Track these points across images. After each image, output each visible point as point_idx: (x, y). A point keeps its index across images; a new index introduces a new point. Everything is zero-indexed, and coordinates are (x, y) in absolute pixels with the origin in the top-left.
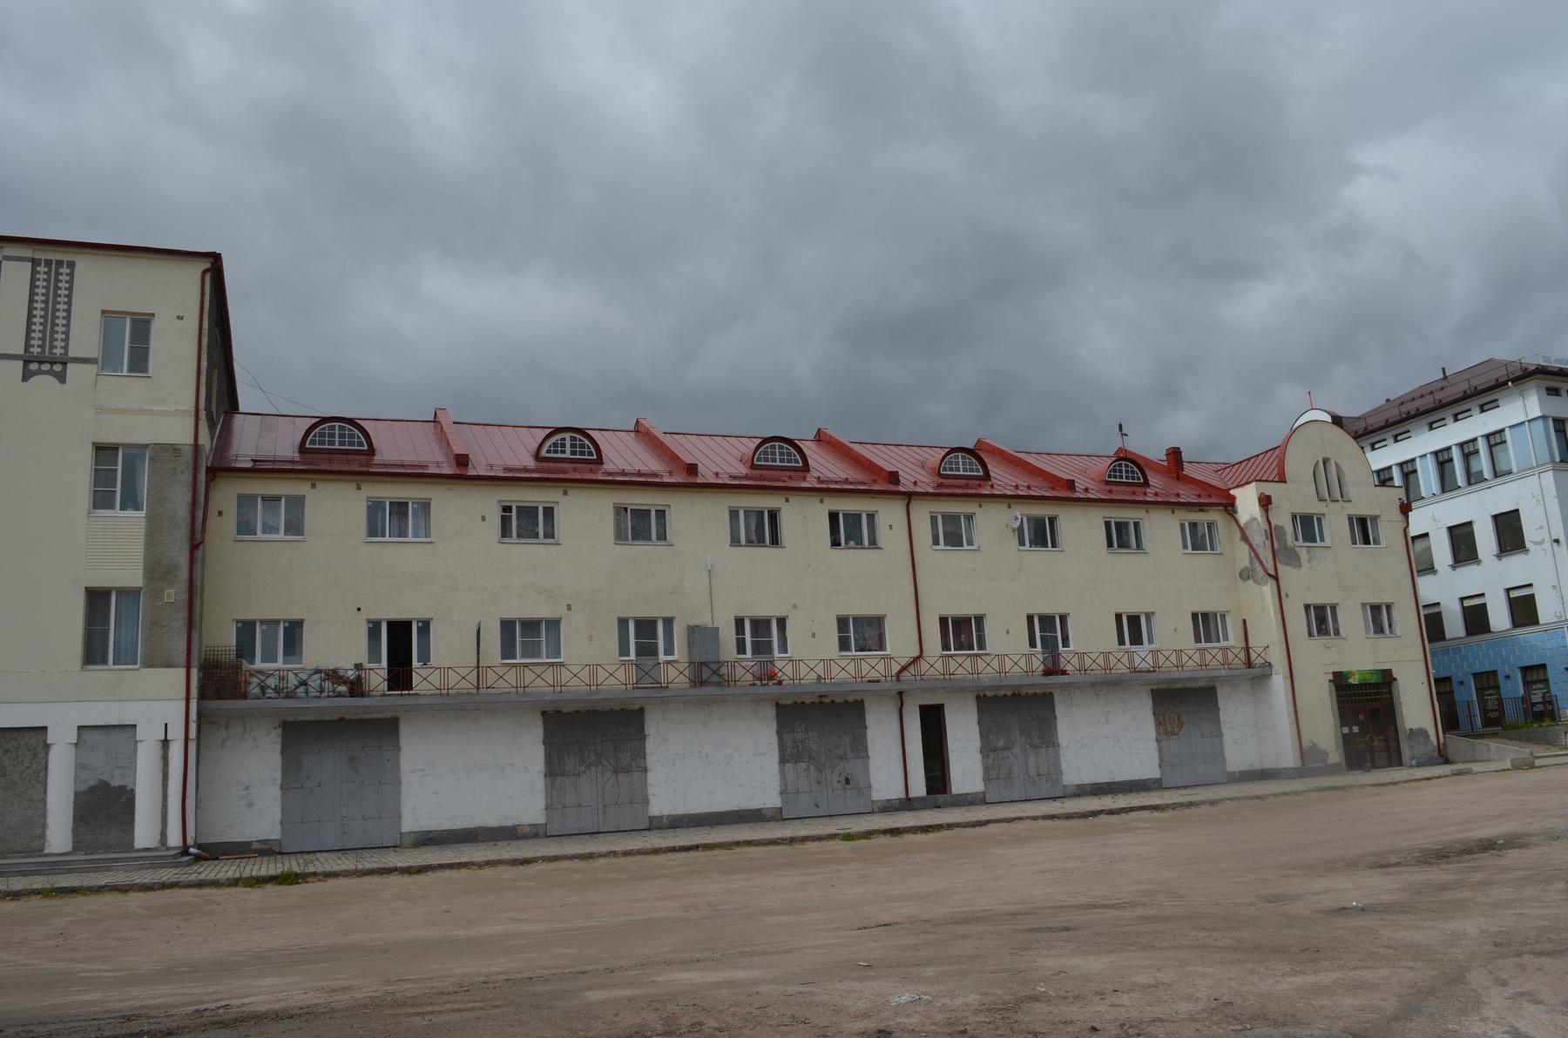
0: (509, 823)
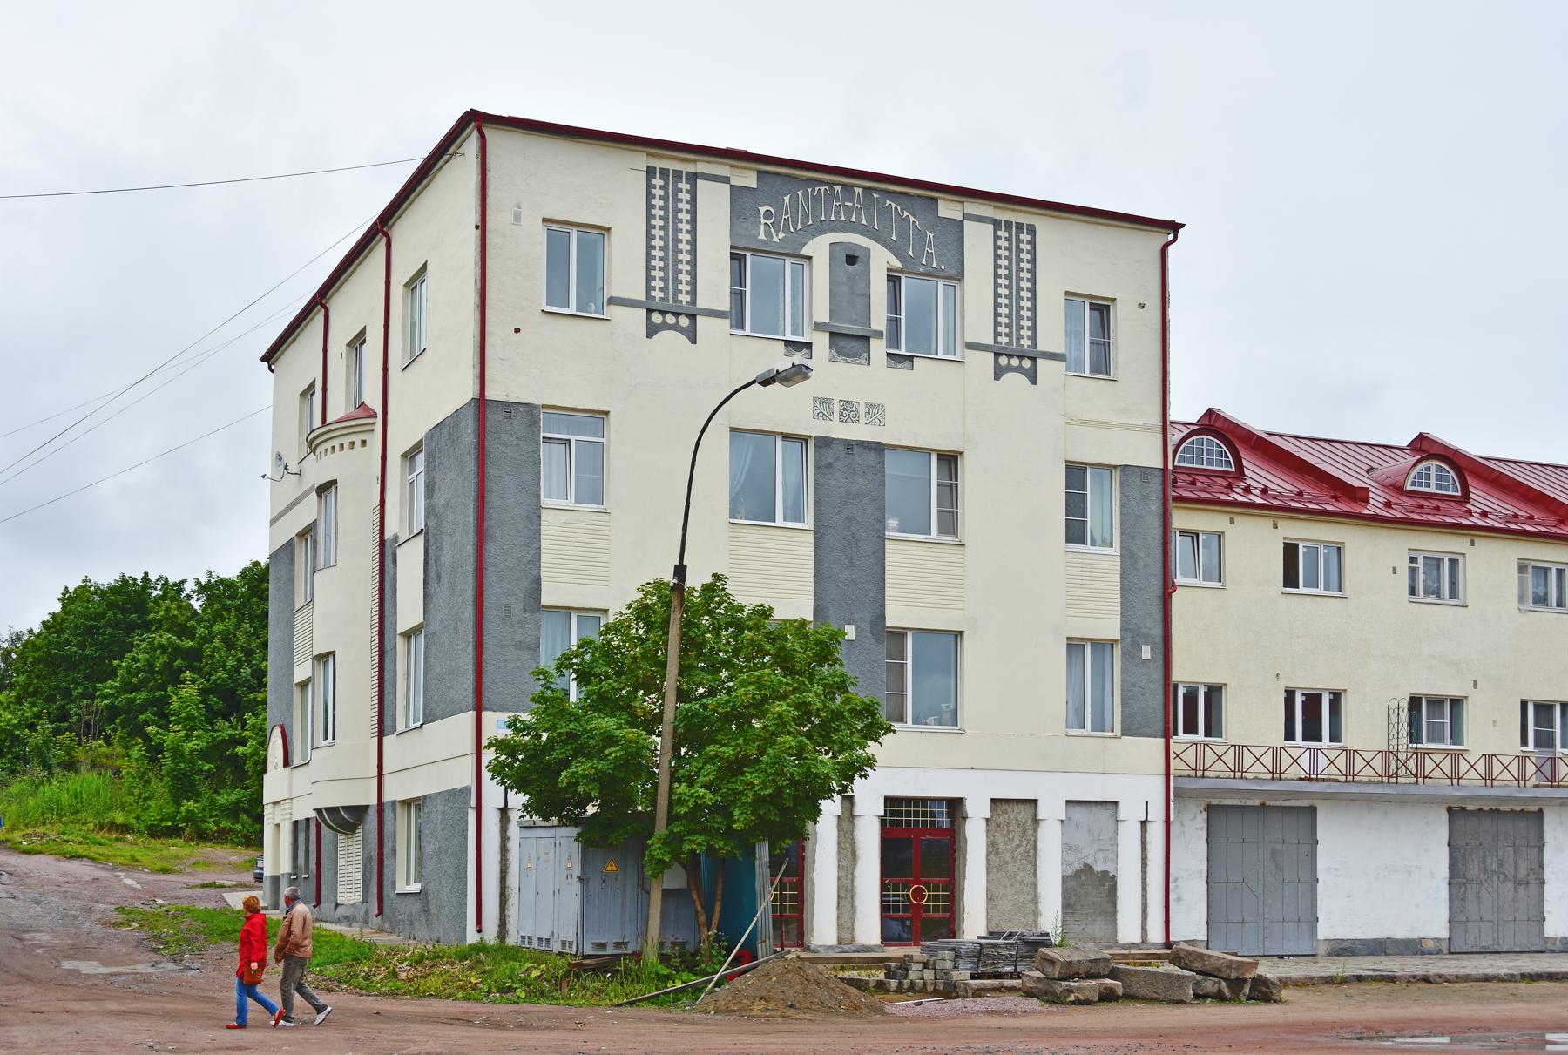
0: (1415, 936)
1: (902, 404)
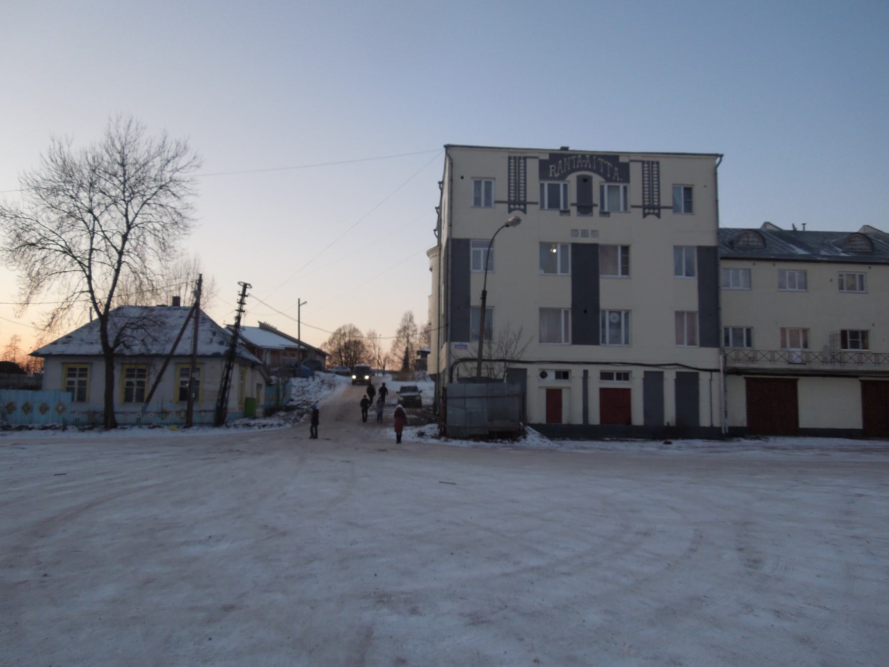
1: (604, 230)
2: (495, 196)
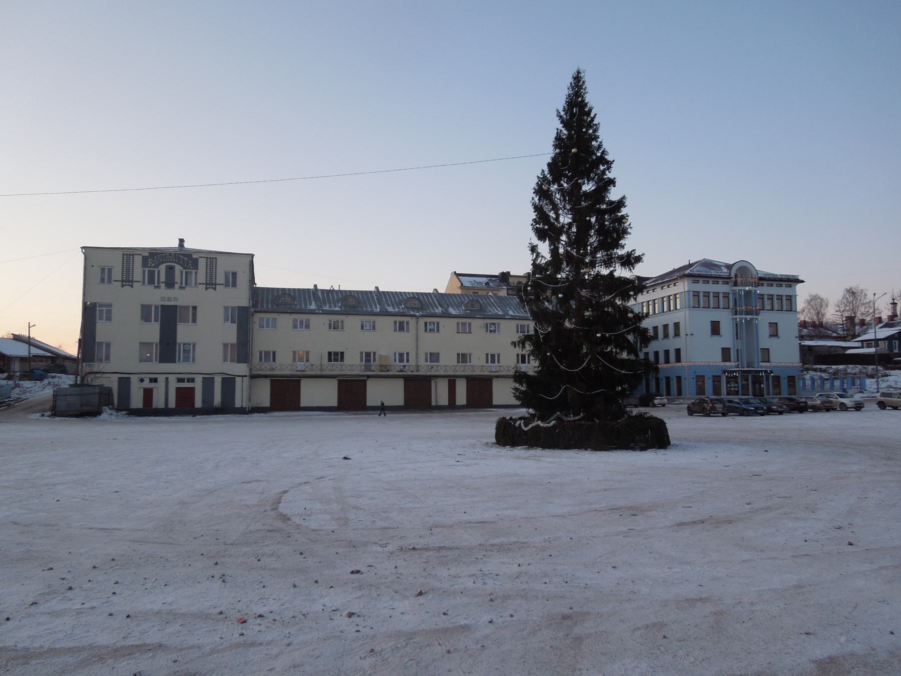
1: (181, 297)
2: (199, 281)
